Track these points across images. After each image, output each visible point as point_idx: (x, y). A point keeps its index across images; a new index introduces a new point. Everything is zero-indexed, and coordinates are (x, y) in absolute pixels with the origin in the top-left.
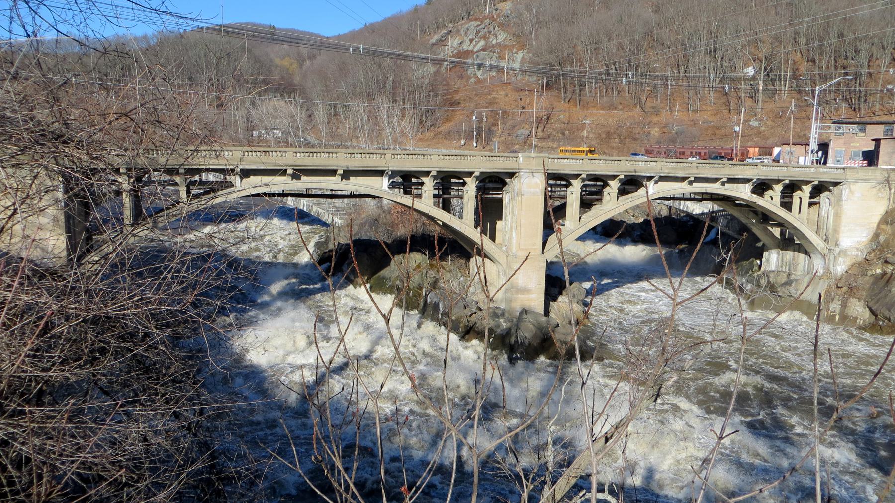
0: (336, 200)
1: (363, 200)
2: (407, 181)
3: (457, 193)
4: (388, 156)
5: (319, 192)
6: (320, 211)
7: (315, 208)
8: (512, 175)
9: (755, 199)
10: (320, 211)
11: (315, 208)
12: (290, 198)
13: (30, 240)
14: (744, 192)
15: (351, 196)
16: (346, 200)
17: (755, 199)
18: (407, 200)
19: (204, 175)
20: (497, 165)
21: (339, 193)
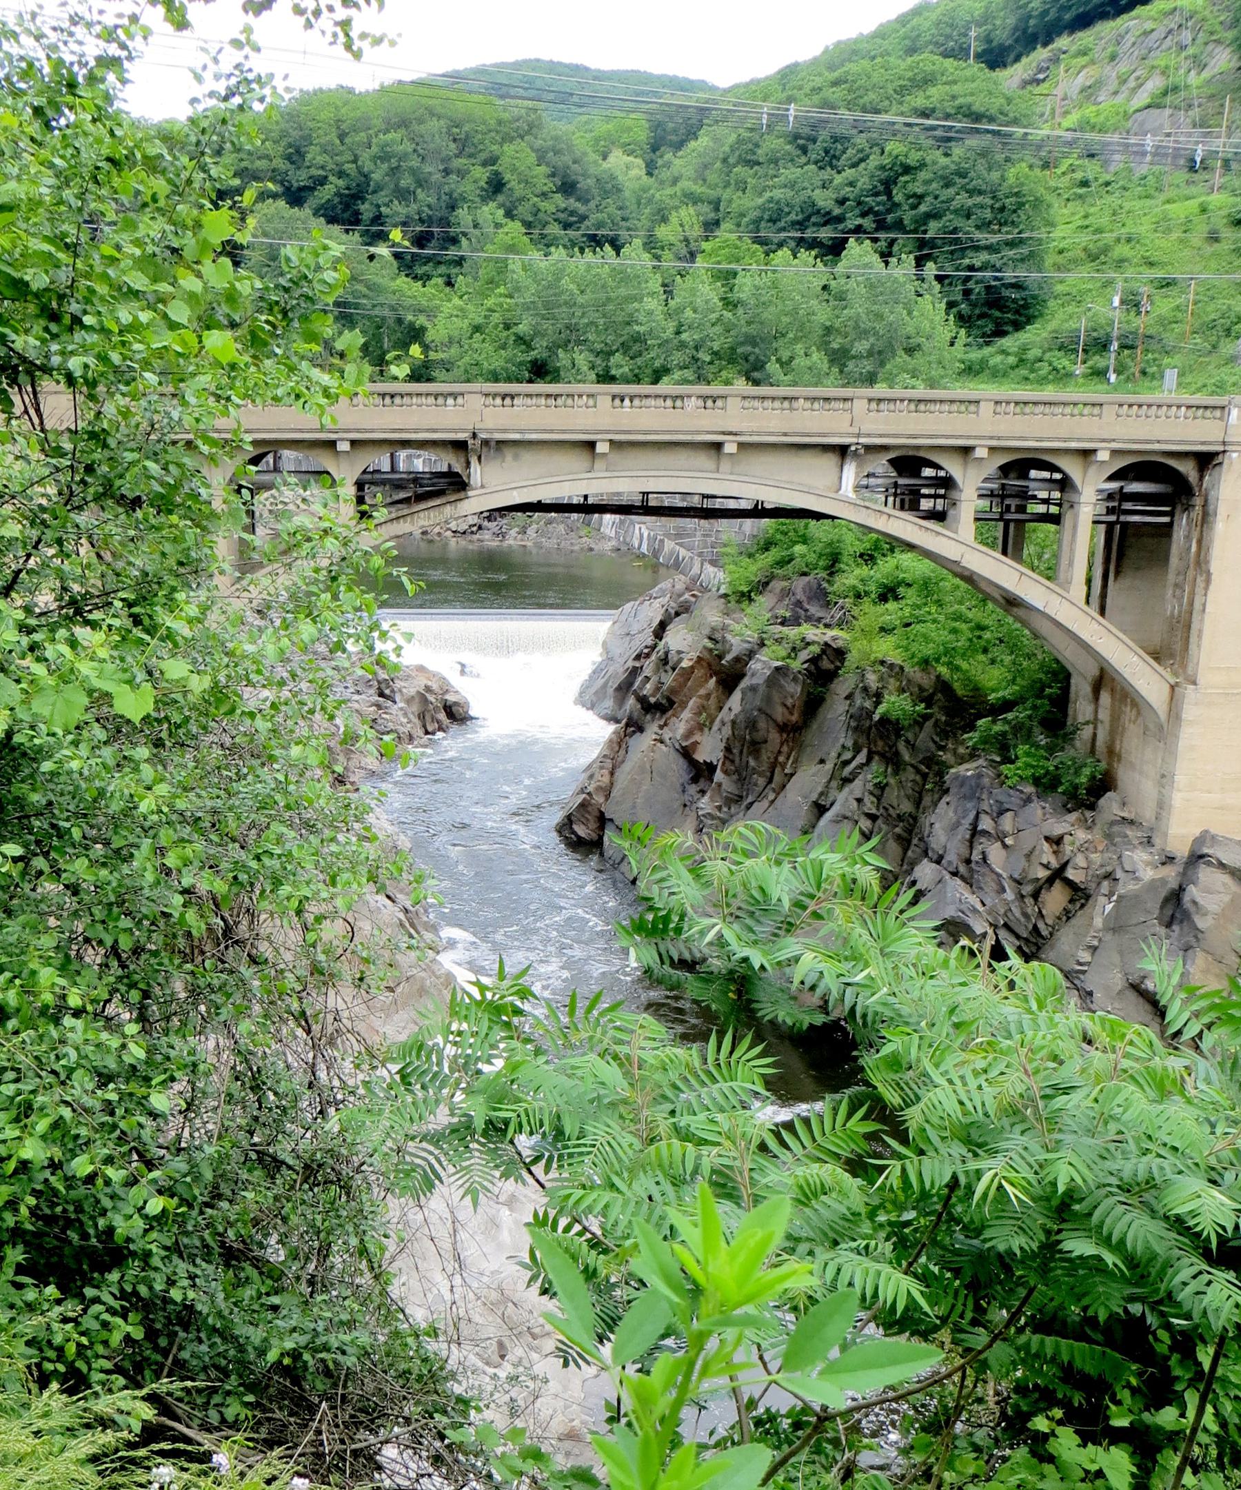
0: (724, 523)
1: (803, 522)
2: (914, 477)
3: (1041, 509)
4: (860, 406)
5: (678, 502)
6: (683, 552)
7: (669, 545)
8: (1206, 460)
9: (1206, 74)
10: (683, 552)
11: (669, 545)
12: (608, 518)
13: (136, 610)
14: (847, 497)
15: (758, 512)
16: (748, 523)
17: (1206, 74)
18: (904, 526)
19: (402, 454)
20: (1166, 430)
21: (732, 504)
